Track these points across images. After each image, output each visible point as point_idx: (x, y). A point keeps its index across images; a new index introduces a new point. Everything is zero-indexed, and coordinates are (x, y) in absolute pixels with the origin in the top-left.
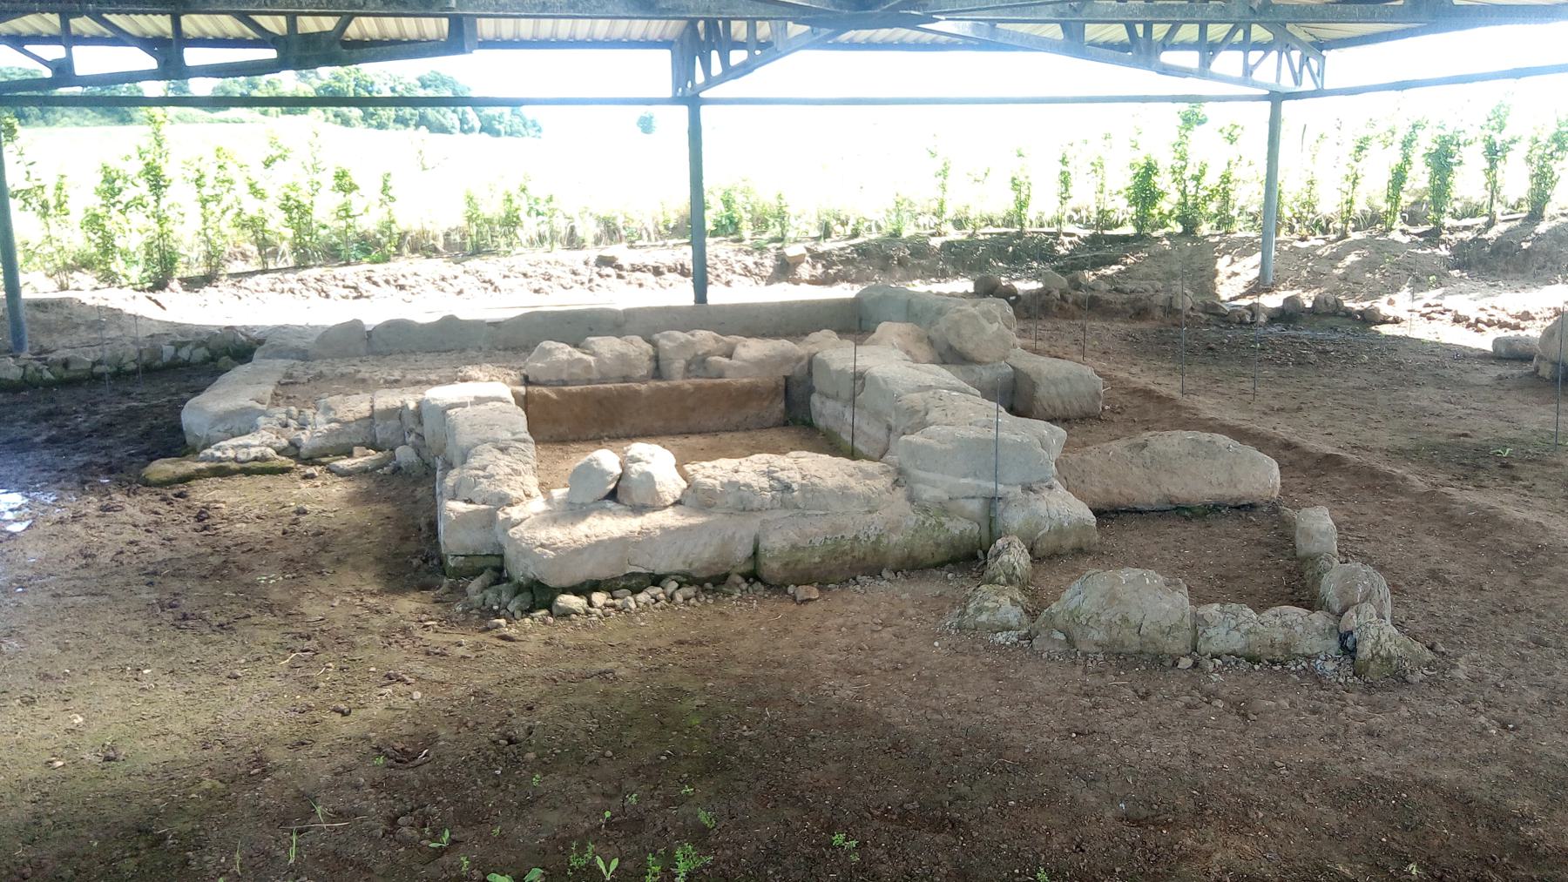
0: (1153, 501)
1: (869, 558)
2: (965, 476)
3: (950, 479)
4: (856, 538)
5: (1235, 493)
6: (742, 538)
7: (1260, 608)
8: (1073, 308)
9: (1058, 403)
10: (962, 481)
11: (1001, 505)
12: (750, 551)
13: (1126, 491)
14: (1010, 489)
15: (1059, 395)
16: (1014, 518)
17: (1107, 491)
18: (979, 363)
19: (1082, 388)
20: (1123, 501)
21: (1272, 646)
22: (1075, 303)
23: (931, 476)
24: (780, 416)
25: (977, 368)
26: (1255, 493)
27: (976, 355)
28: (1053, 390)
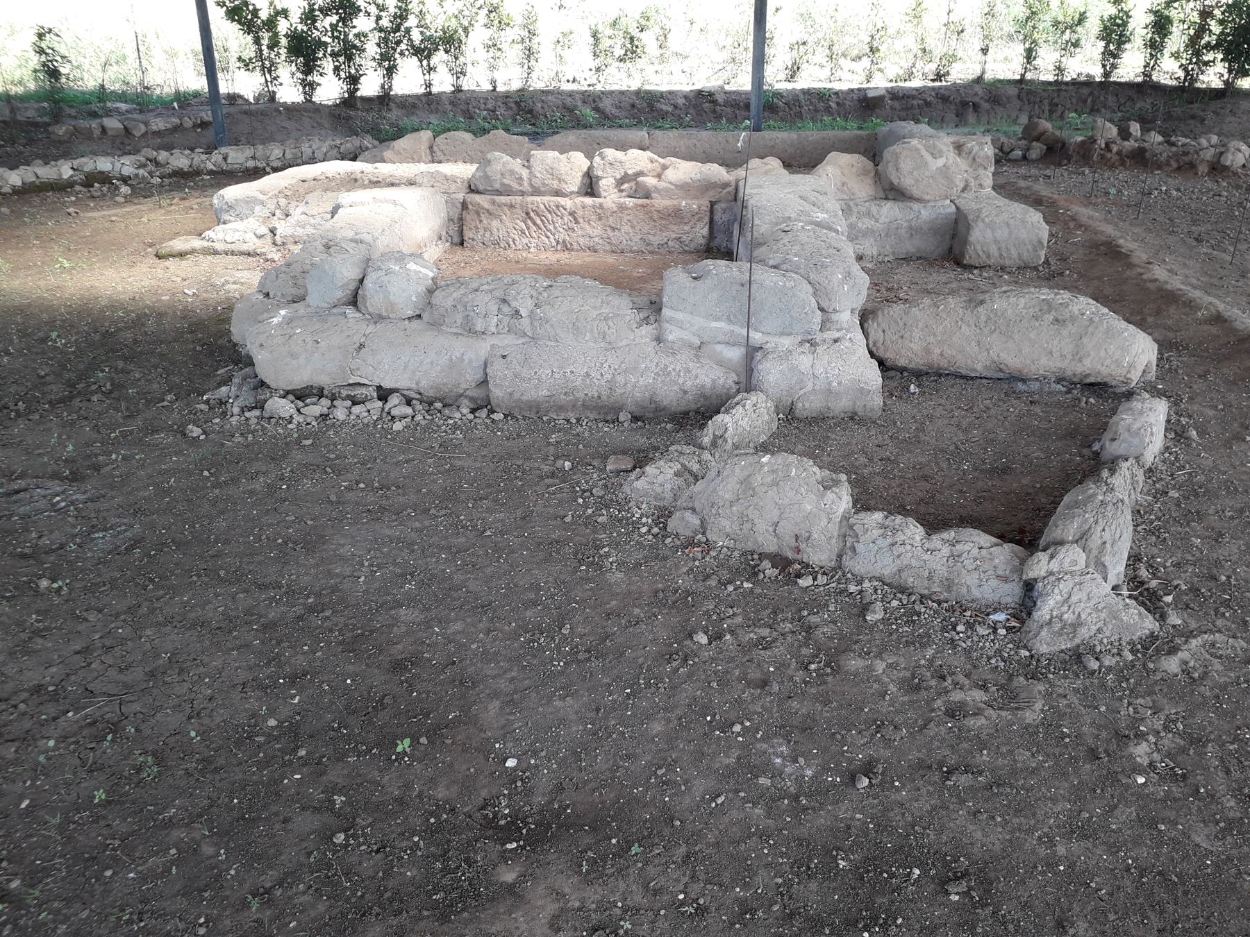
0: (979, 367)
1: (604, 398)
2: (718, 319)
3: (699, 321)
4: (588, 375)
5: (1079, 369)
6: (471, 361)
7: (933, 525)
8: (1116, 158)
9: (994, 250)
10: (715, 324)
11: (759, 355)
12: (479, 376)
13: (948, 352)
14: (766, 338)
15: (996, 241)
16: (771, 373)
17: (927, 351)
18: (918, 200)
19: (1023, 235)
20: (944, 363)
21: (929, 578)
22: (1119, 153)
23: (680, 316)
24: (703, 241)
25: (916, 206)
26: (1104, 371)
27: (916, 192)
28: (989, 234)
